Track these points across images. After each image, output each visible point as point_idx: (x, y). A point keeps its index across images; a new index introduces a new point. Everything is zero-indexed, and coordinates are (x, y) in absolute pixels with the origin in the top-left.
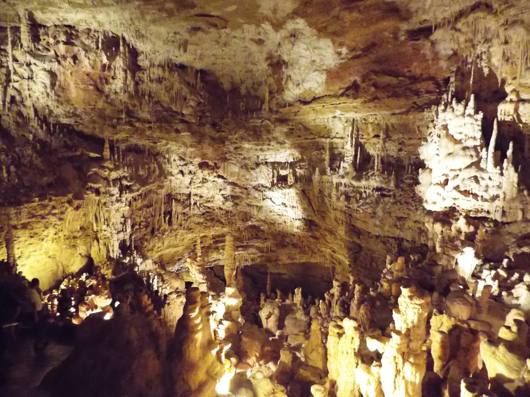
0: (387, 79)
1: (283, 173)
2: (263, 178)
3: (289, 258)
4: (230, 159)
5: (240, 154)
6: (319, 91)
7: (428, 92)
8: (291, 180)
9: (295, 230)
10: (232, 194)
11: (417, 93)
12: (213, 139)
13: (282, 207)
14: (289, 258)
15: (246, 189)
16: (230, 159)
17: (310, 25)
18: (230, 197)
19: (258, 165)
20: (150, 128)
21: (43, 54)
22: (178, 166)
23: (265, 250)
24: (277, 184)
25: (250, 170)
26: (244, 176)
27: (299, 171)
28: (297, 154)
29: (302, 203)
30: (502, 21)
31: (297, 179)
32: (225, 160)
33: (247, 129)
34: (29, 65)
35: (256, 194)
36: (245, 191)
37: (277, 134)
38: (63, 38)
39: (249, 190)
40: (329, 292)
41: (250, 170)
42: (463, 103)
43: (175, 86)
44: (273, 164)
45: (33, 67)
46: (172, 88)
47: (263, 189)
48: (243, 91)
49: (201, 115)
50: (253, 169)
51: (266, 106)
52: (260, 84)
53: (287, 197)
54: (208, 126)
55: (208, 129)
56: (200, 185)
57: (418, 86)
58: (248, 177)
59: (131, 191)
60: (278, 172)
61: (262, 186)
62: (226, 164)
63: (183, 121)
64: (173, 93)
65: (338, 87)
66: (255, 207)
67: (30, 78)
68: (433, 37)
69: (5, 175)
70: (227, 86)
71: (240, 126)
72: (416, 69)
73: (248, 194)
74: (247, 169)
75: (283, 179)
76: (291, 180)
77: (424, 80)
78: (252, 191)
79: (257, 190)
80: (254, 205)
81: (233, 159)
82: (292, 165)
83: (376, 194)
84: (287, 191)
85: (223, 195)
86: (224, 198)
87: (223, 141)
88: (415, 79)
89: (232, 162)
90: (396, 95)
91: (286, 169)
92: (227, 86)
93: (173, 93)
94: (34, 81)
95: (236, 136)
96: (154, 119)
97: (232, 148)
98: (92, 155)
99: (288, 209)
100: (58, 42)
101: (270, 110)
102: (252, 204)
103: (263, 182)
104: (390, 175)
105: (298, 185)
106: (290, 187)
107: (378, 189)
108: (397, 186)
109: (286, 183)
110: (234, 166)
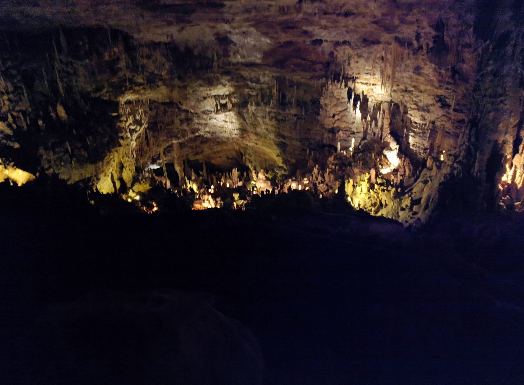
0: (300, 61)
1: (223, 102)
3: (209, 149)
6: (258, 61)
7: (321, 70)
8: (229, 106)
9: (233, 136)
11: (315, 70)
12: (179, 87)
13: (223, 123)
14: (209, 149)
17: (257, 30)
19: (205, 98)
20: (144, 88)
23: (195, 147)
24: (221, 110)
27: (233, 100)
28: (232, 90)
29: (239, 120)
30: (356, 53)
31: (233, 106)
32: (186, 99)
33: (203, 80)
34: (72, 63)
35: (205, 116)
37: (223, 81)
42: (340, 83)
43: (158, 59)
44: (215, 96)
46: (156, 61)
47: (209, 113)
48: (196, 53)
49: (170, 72)
51: (215, 64)
52: (207, 48)
53: (228, 117)
54: (176, 80)
55: (176, 82)
57: (315, 66)
59: (136, 132)
60: (219, 102)
61: (208, 111)
63: (161, 80)
64: (157, 64)
65: (270, 60)
67: (75, 74)
68: (322, 45)
69: (89, 143)
70: (182, 49)
71: (199, 78)
72: (313, 57)
75: (224, 106)
76: (229, 106)
77: (318, 63)
78: (202, 115)
79: (204, 113)
82: (229, 96)
83: (295, 118)
84: (228, 113)
87: (185, 87)
88: (313, 63)
90: (304, 70)
91: (225, 99)
92: (182, 49)
93: (157, 64)
95: (196, 84)
96: (145, 82)
97: (191, 91)
98: (114, 114)
99: (228, 124)
101: (218, 66)
103: (208, 108)
104: (302, 108)
105: (235, 109)
106: (230, 110)
107: (295, 115)
108: (306, 114)
109: (227, 108)
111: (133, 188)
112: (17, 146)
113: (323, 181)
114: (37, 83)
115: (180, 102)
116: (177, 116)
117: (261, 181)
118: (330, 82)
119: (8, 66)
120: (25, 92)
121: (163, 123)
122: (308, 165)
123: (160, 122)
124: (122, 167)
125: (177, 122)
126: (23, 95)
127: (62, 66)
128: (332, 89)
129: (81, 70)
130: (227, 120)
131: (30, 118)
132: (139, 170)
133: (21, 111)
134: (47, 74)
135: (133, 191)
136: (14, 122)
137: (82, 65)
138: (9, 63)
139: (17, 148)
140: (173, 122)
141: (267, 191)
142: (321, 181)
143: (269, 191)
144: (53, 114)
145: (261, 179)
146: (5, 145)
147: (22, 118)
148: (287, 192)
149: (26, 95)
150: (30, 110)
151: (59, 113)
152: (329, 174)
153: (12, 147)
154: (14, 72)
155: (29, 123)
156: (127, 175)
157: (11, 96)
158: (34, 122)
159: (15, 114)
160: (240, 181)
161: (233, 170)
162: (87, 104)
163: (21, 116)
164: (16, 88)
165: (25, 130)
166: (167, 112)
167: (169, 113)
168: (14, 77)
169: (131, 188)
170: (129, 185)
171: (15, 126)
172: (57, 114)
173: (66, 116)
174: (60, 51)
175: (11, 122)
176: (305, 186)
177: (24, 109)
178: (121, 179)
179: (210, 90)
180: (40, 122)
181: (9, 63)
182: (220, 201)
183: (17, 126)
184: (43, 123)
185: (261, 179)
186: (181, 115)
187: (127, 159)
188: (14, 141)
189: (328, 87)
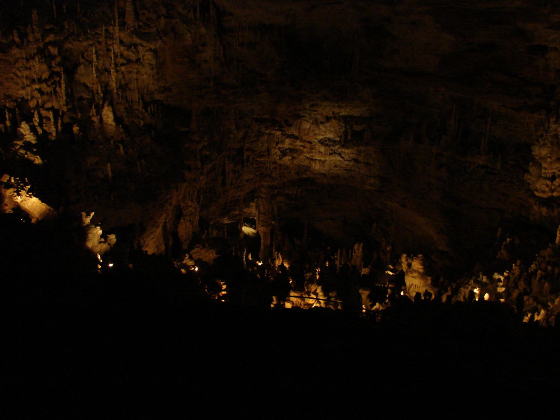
1: (358, 128)
2: (332, 132)
4: (303, 116)
5: (315, 111)
10: (291, 147)
15: (310, 142)
16: (303, 116)
18: (288, 151)
21: (146, 31)
22: (30, 68)
25: (320, 125)
26: (313, 131)
36: (308, 145)
38: (163, 11)
39: (314, 144)
40: (109, 244)
41: (320, 125)
45: (140, 48)
50: (322, 123)
53: (363, 154)
56: (255, 139)
58: (317, 132)
60: (322, 114)
62: (299, 121)
66: (317, 161)
73: (312, 148)
74: (317, 124)
80: (315, 160)
81: (307, 115)
85: (279, 148)
86: (281, 151)
89: (305, 118)
94: (141, 63)
100: (159, 17)
102: (314, 158)
110: (306, 122)
111: (191, 253)
112: (38, 160)
113: (528, 290)
114: (81, 69)
115: (286, 122)
116: (277, 143)
117: (415, 274)
118: (552, 120)
119: (47, 40)
120: (62, 81)
121: (253, 151)
122: (498, 256)
123: (248, 150)
124: (179, 214)
125: (276, 152)
126: (60, 87)
127: (122, 48)
128: (556, 130)
129: (149, 56)
130: (361, 159)
131: (62, 121)
132: (203, 224)
133: (52, 109)
134: (98, 59)
135: (191, 258)
136: (41, 125)
137: (150, 50)
138: (51, 37)
139: (38, 165)
140: (269, 150)
141: (427, 293)
142: (524, 290)
143: (430, 295)
144: (95, 119)
145: (415, 271)
146: (22, 157)
147: (52, 120)
148: (462, 300)
149: (63, 86)
150: (65, 109)
151: (104, 118)
152: (540, 279)
153: (31, 162)
154: (54, 51)
155: (60, 128)
156: (185, 229)
157: (44, 86)
158: (67, 128)
159: (44, 113)
160: (365, 267)
161: (356, 247)
162: (146, 111)
163: (51, 115)
164: (53, 74)
165: (53, 138)
166: (262, 134)
167: (265, 137)
168: (53, 57)
169: (188, 251)
170: (185, 247)
171: (40, 131)
172: (101, 120)
173: (114, 124)
174: (123, 25)
175: (36, 124)
176: (500, 295)
177: (56, 107)
178: (175, 234)
179: (339, 107)
180: (76, 129)
181: (51, 37)
182: (336, 297)
183: (44, 131)
184: (80, 130)
185: (415, 271)
186: (283, 142)
187: (190, 203)
188: (35, 154)
189: (549, 127)
